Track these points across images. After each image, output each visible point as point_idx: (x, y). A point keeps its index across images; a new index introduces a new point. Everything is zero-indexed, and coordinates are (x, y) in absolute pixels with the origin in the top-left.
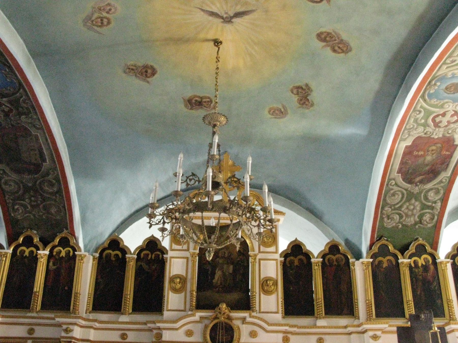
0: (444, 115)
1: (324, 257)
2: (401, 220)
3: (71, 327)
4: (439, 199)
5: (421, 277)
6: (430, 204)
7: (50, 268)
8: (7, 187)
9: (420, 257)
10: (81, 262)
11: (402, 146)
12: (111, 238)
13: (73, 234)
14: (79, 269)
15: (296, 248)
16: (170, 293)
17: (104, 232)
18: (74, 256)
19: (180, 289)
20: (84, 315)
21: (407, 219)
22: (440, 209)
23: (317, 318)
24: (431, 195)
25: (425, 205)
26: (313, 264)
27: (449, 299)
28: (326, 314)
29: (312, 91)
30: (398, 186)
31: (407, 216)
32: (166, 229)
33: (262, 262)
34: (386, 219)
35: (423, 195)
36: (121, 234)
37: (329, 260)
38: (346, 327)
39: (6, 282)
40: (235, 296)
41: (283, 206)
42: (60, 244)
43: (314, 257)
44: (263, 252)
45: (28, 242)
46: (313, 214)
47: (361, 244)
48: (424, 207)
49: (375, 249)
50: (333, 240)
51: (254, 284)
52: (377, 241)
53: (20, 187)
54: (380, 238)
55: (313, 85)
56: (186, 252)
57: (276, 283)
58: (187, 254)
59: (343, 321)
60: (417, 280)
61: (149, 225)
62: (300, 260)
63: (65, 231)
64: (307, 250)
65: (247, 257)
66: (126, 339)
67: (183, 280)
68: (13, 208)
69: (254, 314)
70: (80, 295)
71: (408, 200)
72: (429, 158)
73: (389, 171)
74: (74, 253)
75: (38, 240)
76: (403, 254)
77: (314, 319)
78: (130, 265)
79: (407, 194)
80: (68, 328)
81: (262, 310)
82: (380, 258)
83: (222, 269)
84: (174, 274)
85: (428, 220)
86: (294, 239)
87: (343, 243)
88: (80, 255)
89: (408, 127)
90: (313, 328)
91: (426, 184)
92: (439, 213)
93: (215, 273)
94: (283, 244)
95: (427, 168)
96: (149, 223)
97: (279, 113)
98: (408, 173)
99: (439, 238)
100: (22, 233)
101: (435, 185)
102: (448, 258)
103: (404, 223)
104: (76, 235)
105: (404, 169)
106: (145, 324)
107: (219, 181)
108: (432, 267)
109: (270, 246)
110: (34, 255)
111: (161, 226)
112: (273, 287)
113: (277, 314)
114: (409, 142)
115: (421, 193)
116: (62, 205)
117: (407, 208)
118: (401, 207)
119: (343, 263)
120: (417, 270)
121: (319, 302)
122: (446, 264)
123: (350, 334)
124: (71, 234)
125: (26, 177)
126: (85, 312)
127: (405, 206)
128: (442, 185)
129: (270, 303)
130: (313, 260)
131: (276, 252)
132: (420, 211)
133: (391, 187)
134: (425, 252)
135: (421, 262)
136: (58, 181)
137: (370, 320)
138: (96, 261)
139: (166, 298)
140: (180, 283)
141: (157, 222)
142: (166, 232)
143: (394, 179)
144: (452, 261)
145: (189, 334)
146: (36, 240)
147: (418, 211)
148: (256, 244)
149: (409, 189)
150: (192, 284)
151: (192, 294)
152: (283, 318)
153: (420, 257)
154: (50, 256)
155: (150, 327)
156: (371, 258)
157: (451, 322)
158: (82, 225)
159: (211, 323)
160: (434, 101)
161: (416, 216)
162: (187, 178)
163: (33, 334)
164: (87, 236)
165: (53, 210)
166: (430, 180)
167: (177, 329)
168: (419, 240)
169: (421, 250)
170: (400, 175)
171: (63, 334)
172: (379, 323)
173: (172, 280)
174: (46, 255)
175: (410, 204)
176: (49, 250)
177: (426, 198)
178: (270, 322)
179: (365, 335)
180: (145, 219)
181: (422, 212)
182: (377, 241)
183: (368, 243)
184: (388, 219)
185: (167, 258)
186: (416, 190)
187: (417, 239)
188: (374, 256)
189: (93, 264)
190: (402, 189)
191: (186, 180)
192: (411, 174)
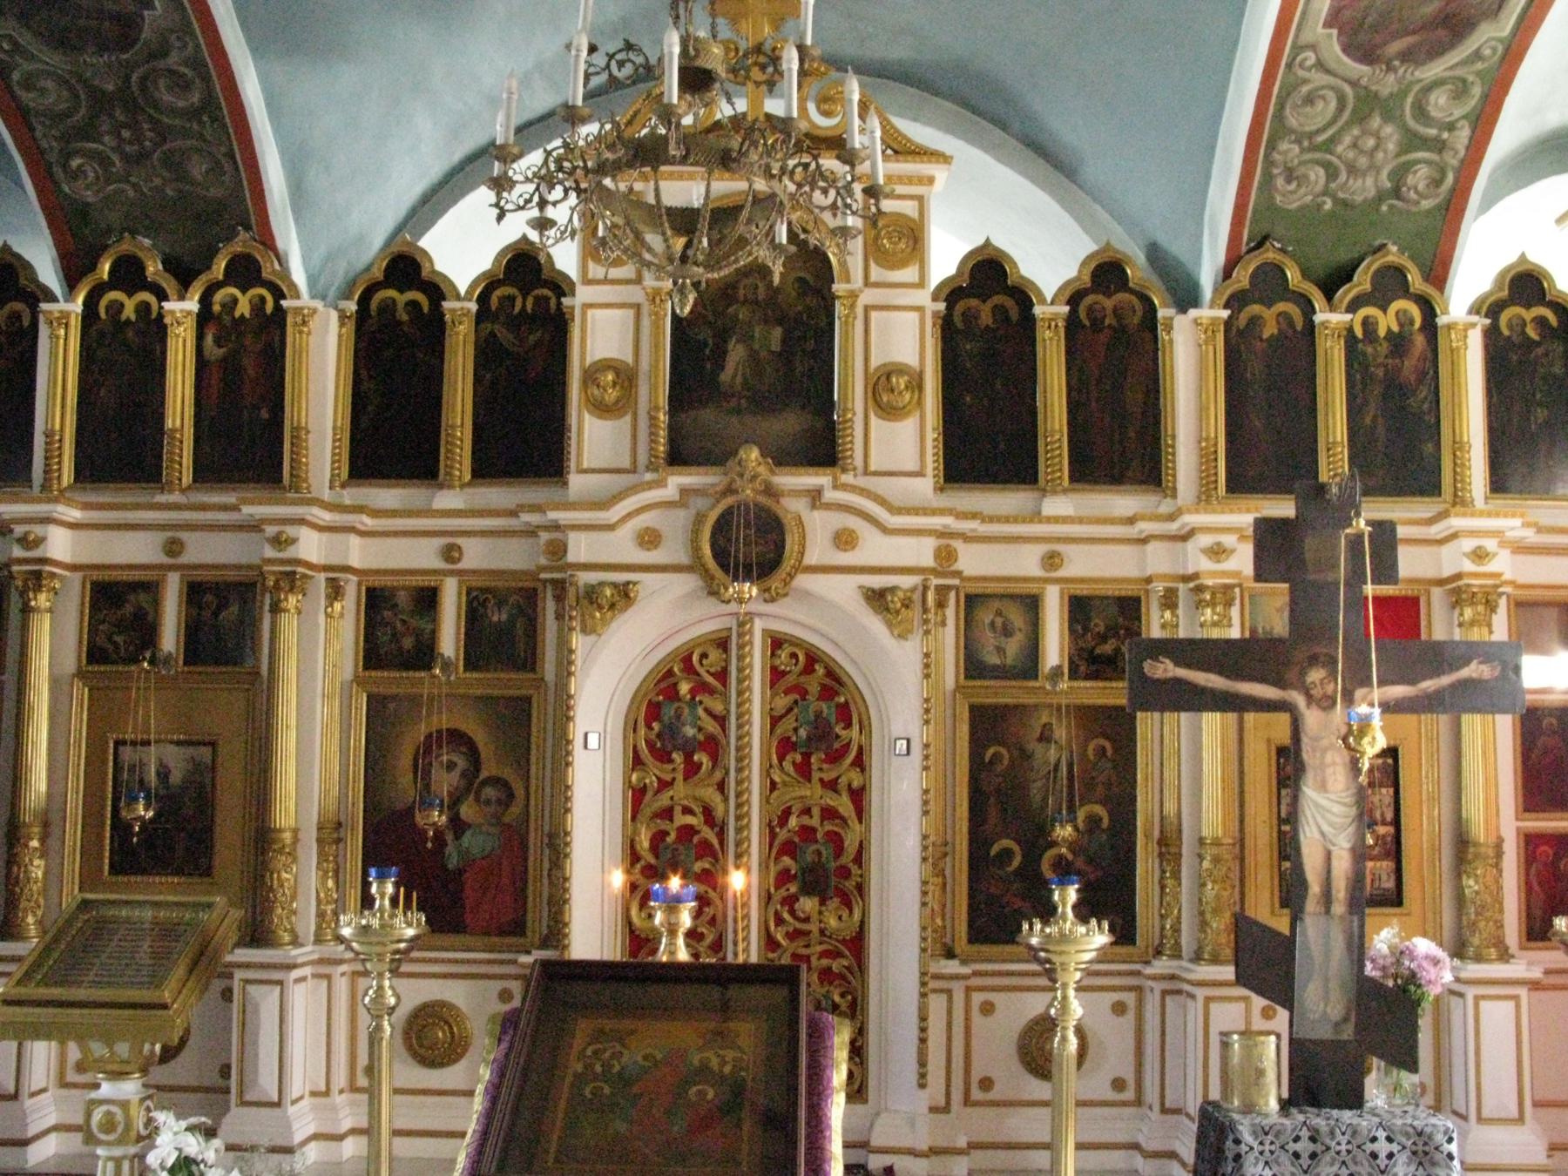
1: (1074, 300)
2: (1333, 185)
3: (290, 531)
4: (1463, 117)
5: (1380, 372)
6: (1433, 132)
7: (206, 353)
8: (31, 95)
10: (301, 332)
12: (395, 249)
13: (268, 241)
14: (299, 353)
15: (988, 272)
16: (587, 416)
17: (369, 231)
18: (280, 312)
19: (617, 402)
20: (326, 495)
21: (1351, 181)
22: (1467, 148)
23: (1044, 490)
24: (1439, 102)
25: (1415, 135)
26: (1039, 324)
27: (1461, 442)
28: (1072, 479)
31: (1352, 170)
32: (552, 223)
33: (874, 315)
34: (1280, 182)
35: (1410, 100)
36: (422, 234)
37: (1090, 309)
38: (1131, 521)
39: (79, 403)
40: (790, 423)
41: (948, 130)
42: (231, 276)
43: (1043, 301)
44: (877, 285)
45: (129, 275)
46: (1047, 158)
47: (1198, 263)
48: (1412, 141)
50: (1108, 247)
51: (851, 389)
52: (1248, 252)
53: (77, 96)
54: (1260, 243)
56: (630, 287)
57: (917, 384)
58: (635, 294)
59: (1123, 502)
60: (1367, 377)
61: (496, 211)
62: (999, 310)
63: (243, 235)
64: (1022, 277)
65: (827, 302)
66: (459, 560)
67: (626, 376)
68: (65, 166)
69: (847, 478)
70: (308, 432)
71: (1360, 118)
73: (1298, 14)
74: (276, 302)
75: (160, 267)
76: (1329, 295)
77: (1036, 494)
78: (457, 334)
79: (1357, 98)
80: (280, 533)
81: (872, 468)
82: (1256, 309)
83: (747, 339)
84: (597, 358)
85: (1421, 187)
86: (981, 242)
87: (1140, 257)
88: (298, 311)
90: (1031, 521)
91: (1423, 63)
92: (1462, 161)
93: (725, 352)
94: (945, 257)
96: (497, 205)
98: (1361, 25)
99: (1453, 249)
100: (105, 247)
101: (1451, 68)
102: (1478, 313)
103: (1341, 195)
104: (280, 244)
105: (1347, 14)
106: (513, 513)
107: (708, 66)
108: (1420, 341)
109: (902, 264)
110: (154, 315)
111: (535, 213)
112: (907, 396)
113: (918, 480)
116: (223, 149)
117: (1355, 145)
118: (1333, 140)
119: (1136, 320)
120: (1370, 350)
121: (1052, 443)
122: (1466, 330)
123: (1144, 541)
124: (263, 243)
125: (91, 58)
126: (327, 484)
127: (1347, 140)
128: (1479, 66)
129: (899, 446)
130: (1038, 310)
132: (1398, 155)
133: (1301, 73)
134: (1404, 291)
135: (1386, 322)
136: (197, 64)
137: (1208, 501)
138: (351, 326)
139: (574, 435)
140: (615, 384)
141: (521, 203)
142: (552, 232)
143: (1313, 47)
144: (1488, 321)
145: (650, 542)
146: (153, 268)
147: (1390, 156)
148: (856, 263)
149: (1364, 81)
150: (653, 389)
151: (653, 419)
154: (204, 317)
155: (528, 524)
156: (1226, 306)
157: (1458, 508)
158: (294, 211)
159: (713, 506)
162: (611, 57)
163: (180, 553)
164: (315, 248)
165: (198, 169)
166: (1436, 52)
167: (611, 527)
168: (1388, 253)
169: (1391, 284)
170: (1335, 32)
171: (269, 552)
172: (1232, 511)
173: (591, 376)
174: (189, 313)
175: (1364, 132)
176: (197, 298)
177: (1421, 112)
178: (897, 504)
179: (1190, 545)
180: (483, 196)
181: (1404, 158)
182: (1248, 252)
183: (1221, 258)
184: (1289, 181)
185: (573, 308)
186: (1387, 84)
187: (1383, 246)
188: (1235, 302)
189: (340, 336)
190: (1339, 82)
191: (608, 66)
192: (1375, 28)
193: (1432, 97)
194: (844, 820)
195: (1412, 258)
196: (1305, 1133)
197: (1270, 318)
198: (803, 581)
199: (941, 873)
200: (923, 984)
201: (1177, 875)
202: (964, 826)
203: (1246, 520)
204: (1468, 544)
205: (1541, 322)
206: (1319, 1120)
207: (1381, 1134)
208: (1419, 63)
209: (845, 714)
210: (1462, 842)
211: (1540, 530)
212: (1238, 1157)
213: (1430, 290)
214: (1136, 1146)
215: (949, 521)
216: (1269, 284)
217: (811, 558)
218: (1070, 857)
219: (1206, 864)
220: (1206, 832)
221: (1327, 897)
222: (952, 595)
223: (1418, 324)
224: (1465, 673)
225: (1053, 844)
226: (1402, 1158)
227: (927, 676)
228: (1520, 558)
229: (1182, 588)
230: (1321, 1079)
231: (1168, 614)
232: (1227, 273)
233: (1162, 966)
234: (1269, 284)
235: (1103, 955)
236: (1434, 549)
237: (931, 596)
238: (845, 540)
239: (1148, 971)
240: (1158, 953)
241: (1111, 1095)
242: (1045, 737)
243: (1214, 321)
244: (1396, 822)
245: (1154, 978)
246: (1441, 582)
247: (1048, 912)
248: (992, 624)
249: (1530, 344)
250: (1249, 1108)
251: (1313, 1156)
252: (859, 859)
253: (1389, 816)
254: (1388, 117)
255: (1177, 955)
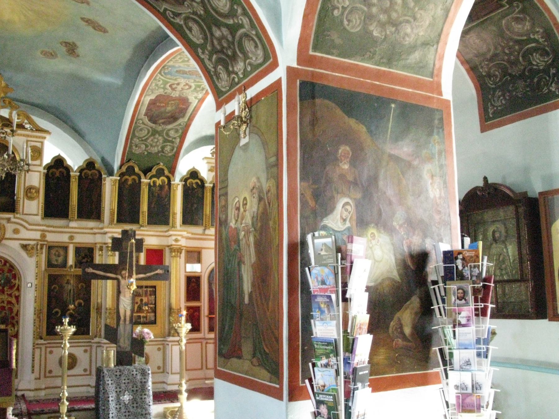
0: (178, 84)
6: (171, 139)
9: (158, 178)
11: (147, 100)
15: (59, 162)
24: (172, 133)
29: (78, 47)
30: (145, 124)
34: (134, 147)
38: (92, 229)
46: (77, 133)
47: (114, 161)
48: (166, 141)
49: (124, 169)
55: (78, 43)
57: (38, 191)
59: (91, 224)
69: (18, 216)
72: (169, 109)
76: (145, 175)
81: (25, 212)
82: (127, 177)
89: (151, 88)
94: (47, 159)
95: (169, 114)
97: (52, 55)
101: (176, 126)
105: (149, 114)
108: (167, 187)
114: (153, 97)
115: (163, 131)
117: (152, 140)
118: (147, 139)
123: (95, 234)
127: (150, 139)
128: (180, 126)
129: (33, 207)
130: (72, 174)
131: (40, 165)
135: (159, 182)
143: (141, 119)
152: (43, 219)
153: (158, 178)
157: (173, 229)
160: (169, 76)
161: (160, 147)
166: (170, 123)
169: (160, 173)
177: (167, 134)
183: (119, 163)
186: (159, 128)
188: (122, 175)
193: (170, 132)
194: (13, 304)
195: (166, 167)
196: (118, 371)
197: (130, 179)
198: (4, 242)
199: (39, 317)
200: (34, 346)
201: (101, 317)
202: (46, 305)
203: (120, 230)
204: (174, 238)
205: (197, 183)
206: (121, 368)
207: (135, 370)
208: (166, 125)
209: (14, 277)
210: (170, 309)
211: (192, 234)
212: (103, 376)
213: (170, 175)
214: (89, 385)
215: (44, 228)
216: (130, 171)
217: (7, 236)
218: (74, 313)
219: (107, 314)
220: (107, 307)
221: (125, 319)
222: (45, 246)
223: (166, 183)
224: (156, 272)
225: (69, 310)
226: (139, 375)
227: (37, 267)
228: (188, 240)
229: (104, 246)
230: (123, 359)
231: (100, 252)
232: (120, 167)
233: (97, 340)
234: (130, 171)
235: (75, 334)
236: (167, 238)
237: (39, 247)
238: (16, 231)
239: (93, 341)
240: (96, 337)
241: (83, 373)
242: (68, 282)
243: (116, 180)
244: (155, 304)
245: (94, 343)
246: (168, 246)
247: (62, 324)
248: (55, 253)
249: (193, 189)
250: (108, 366)
251: (120, 375)
252: (17, 315)
253: (153, 303)
254: (159, 135)
255: (100, 337)
